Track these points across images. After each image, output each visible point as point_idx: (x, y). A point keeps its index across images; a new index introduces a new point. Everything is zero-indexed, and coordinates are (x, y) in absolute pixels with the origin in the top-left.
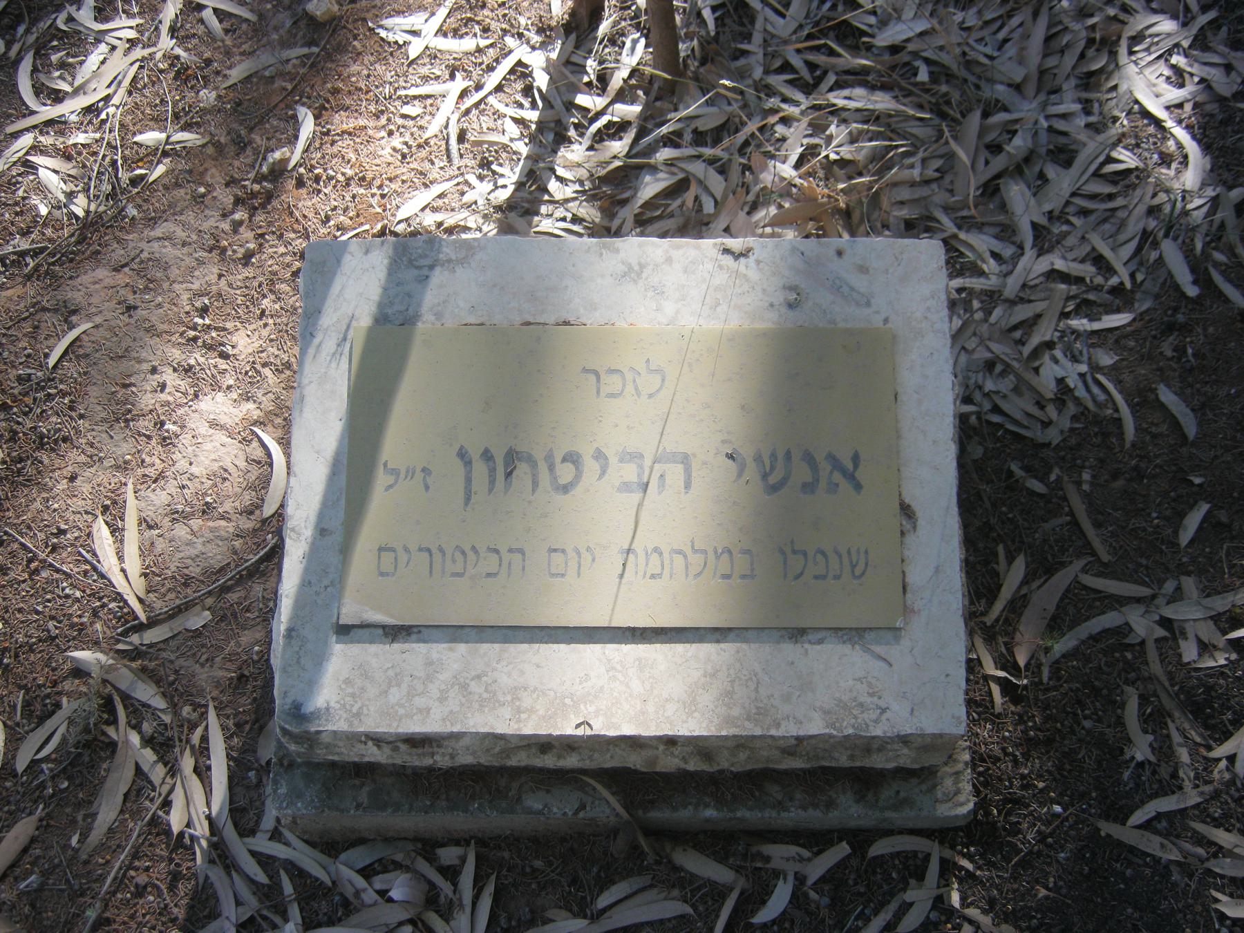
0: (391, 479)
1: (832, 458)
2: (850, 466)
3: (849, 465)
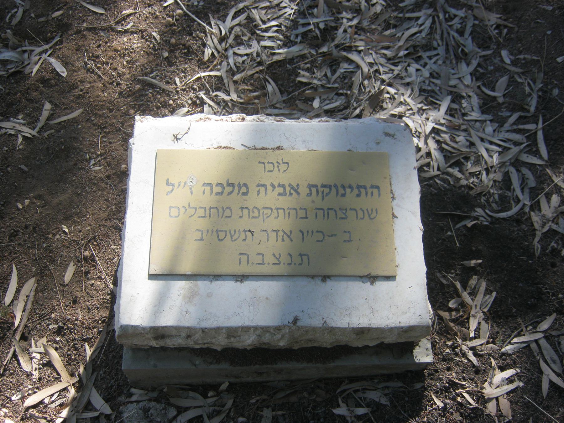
0: (231, 189)
1: (290, 185)
2: (296, 188)
3: (296, 188)
